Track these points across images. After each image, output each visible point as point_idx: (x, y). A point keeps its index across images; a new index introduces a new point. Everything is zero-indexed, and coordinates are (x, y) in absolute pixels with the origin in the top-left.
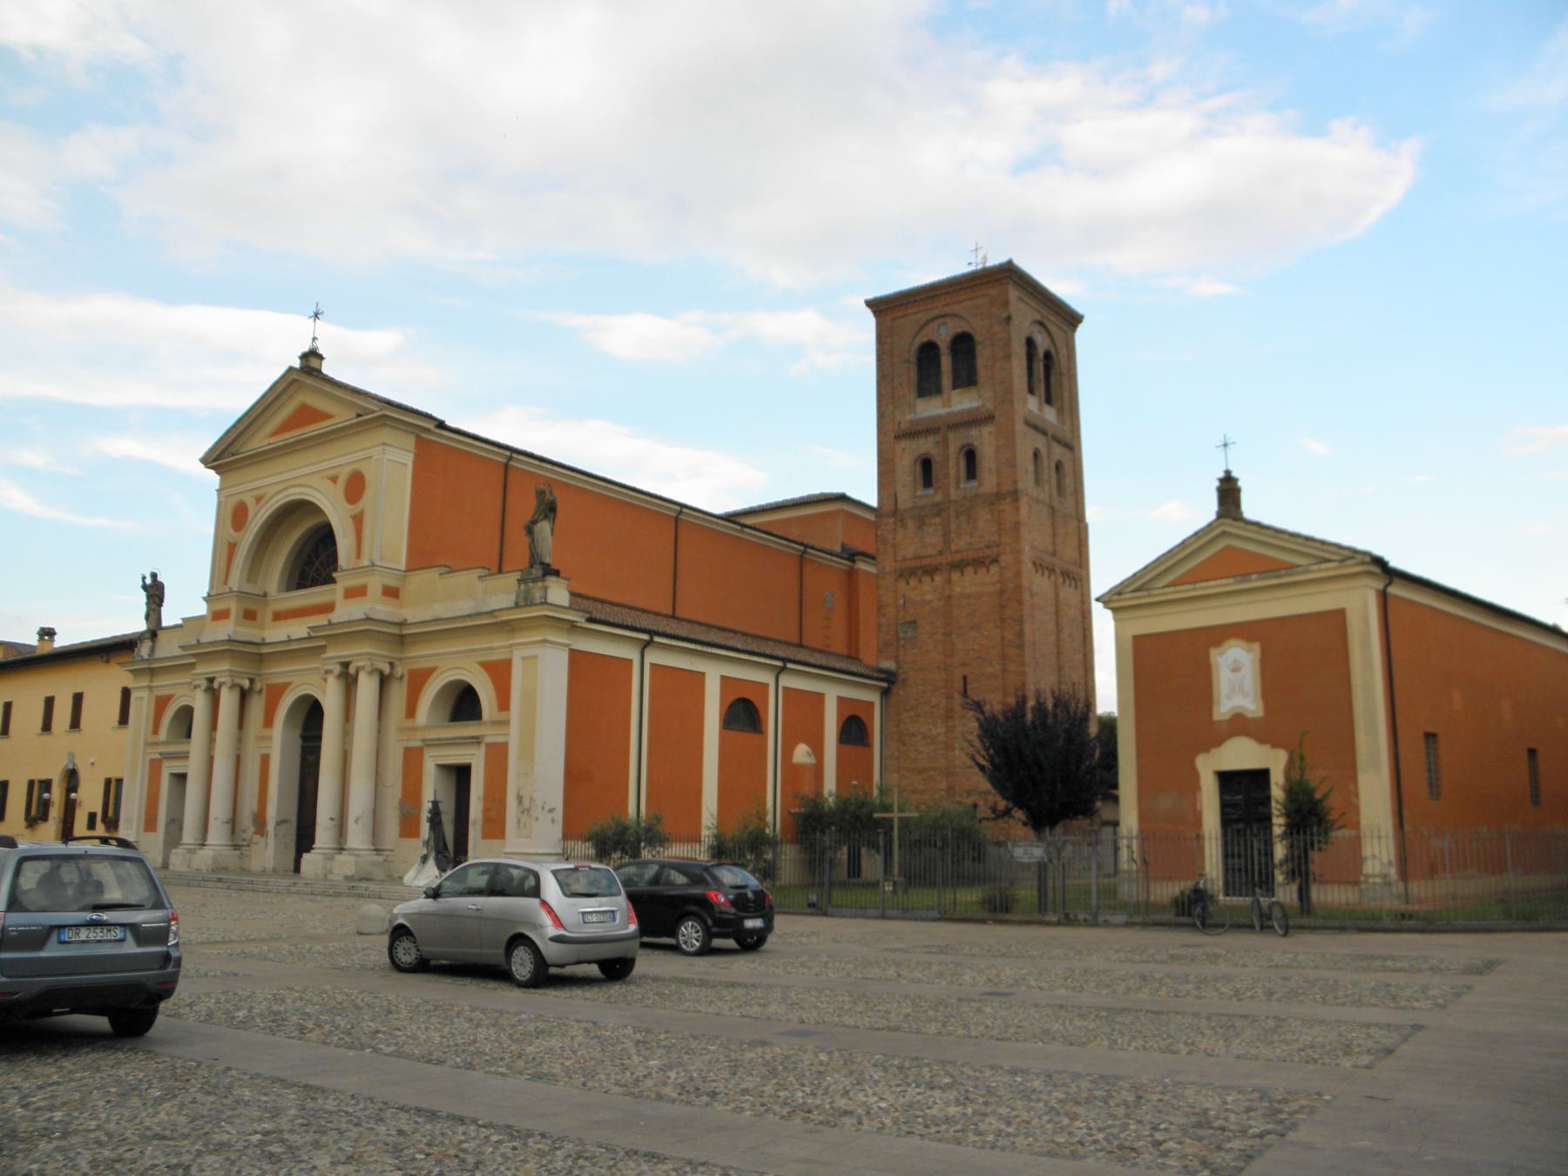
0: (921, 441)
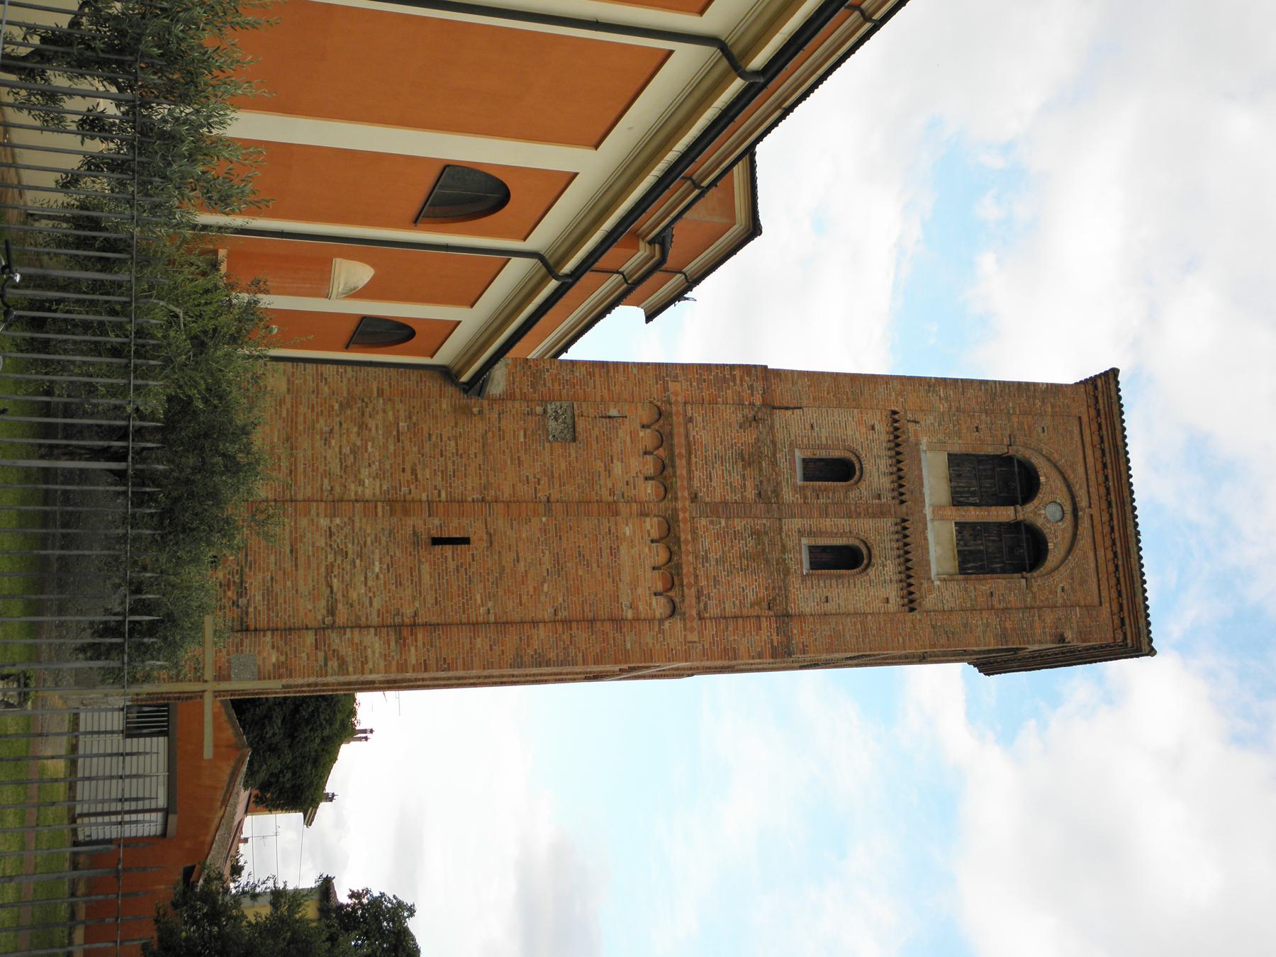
0: (884, 464)
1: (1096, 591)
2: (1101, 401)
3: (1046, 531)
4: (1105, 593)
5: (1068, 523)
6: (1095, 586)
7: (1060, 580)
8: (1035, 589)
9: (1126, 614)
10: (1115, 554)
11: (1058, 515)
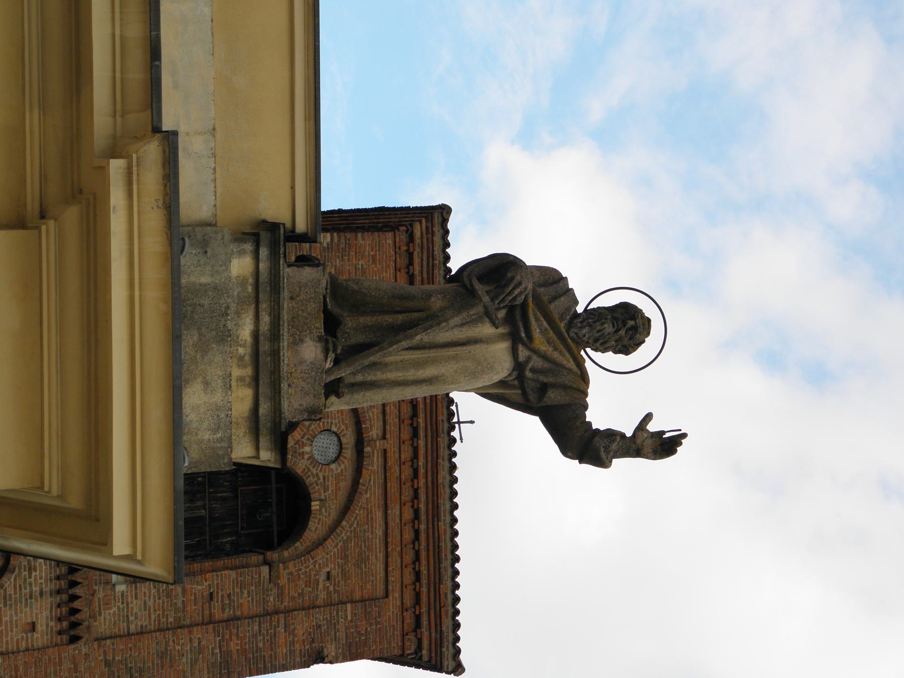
1: (382, 574)
2: (417, 260)
3: (309, 481)
4: (394, 577)
5: (347, 465)
6: (380, 566)
7: (326, 560)
8: (283, 581)
9: (424, 609)
10: (417, 512)
11: (332, 452)
